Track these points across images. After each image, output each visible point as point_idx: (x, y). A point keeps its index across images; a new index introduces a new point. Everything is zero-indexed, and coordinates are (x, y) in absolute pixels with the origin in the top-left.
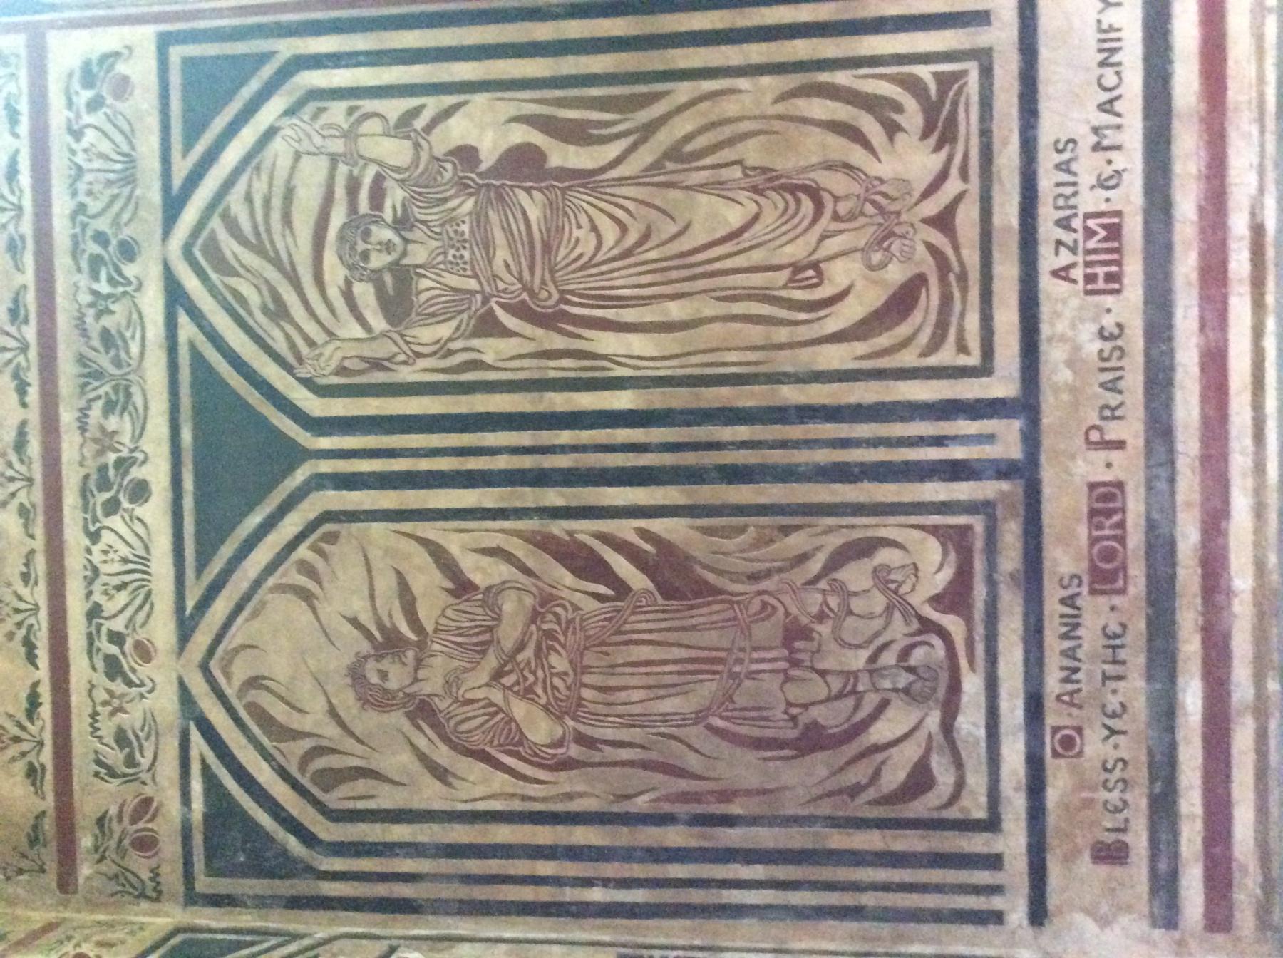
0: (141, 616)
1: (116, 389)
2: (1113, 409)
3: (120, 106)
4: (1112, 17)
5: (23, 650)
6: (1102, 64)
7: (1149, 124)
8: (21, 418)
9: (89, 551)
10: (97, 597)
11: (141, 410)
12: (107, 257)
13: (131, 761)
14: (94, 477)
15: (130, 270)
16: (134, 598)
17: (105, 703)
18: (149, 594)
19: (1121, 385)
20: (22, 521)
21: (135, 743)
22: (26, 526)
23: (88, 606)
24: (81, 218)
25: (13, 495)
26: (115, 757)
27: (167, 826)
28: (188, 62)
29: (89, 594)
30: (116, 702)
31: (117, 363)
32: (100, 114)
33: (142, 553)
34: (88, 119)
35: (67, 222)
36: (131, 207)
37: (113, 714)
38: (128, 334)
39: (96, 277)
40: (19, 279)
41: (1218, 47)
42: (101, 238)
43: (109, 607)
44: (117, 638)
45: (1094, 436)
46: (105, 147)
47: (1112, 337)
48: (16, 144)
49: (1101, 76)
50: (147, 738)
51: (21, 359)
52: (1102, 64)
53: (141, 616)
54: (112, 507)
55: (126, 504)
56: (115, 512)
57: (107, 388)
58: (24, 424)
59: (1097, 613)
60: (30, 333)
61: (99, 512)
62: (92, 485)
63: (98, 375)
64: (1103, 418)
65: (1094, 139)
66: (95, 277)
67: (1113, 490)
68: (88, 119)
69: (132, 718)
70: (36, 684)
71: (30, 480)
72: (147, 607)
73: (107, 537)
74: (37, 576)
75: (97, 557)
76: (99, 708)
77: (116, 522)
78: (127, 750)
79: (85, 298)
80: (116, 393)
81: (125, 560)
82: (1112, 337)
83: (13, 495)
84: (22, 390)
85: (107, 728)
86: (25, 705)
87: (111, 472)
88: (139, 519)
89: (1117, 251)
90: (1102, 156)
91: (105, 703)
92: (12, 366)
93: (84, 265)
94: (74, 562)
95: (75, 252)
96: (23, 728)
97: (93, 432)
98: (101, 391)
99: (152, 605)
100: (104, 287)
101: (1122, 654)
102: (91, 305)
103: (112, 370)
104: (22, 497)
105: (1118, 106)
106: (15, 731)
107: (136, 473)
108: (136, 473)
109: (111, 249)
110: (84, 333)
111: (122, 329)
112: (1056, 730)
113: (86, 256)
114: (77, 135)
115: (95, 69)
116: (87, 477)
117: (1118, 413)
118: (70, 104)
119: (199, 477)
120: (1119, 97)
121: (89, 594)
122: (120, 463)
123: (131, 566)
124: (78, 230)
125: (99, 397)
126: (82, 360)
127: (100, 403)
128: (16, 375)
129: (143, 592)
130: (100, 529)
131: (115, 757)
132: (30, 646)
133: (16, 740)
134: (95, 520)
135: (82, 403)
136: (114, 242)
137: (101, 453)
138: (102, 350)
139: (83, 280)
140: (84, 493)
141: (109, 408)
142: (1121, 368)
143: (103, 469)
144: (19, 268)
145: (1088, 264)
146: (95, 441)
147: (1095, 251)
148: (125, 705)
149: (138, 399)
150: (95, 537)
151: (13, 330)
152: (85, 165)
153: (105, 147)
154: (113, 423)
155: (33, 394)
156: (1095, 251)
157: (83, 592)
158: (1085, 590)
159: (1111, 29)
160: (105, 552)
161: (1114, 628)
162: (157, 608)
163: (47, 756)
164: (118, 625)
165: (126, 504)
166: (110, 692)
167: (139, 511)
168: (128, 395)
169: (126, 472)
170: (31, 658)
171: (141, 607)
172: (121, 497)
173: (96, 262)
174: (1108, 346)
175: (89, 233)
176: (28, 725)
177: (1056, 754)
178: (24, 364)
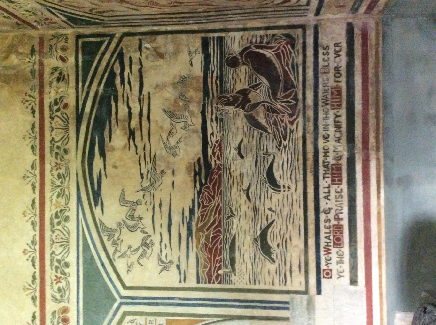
0: (66, 255)
1: (61, 190)
3: (65, 111)
5: (31, 263)
7: (353, 177)
8: (33, 198)
9: (51, 236)
10: (53, 136)
11: (68, 196)
12: (59, 153)
13: (62, 296)
15: (66, 157)
16: (65, 249)
18: (69, 248)
20: (32, 319)
21: (63, 291)
22: (33, 227)
23: (51, 252)
24: (53, 255)
26: (58, 296)
28: (83, 43)
29: (51, 135)
30: (58, 280)
34: (56, 227)
35: (49, 144)
38: (66, 175)
40: (35, 196)
41: (389, 314)
43: (56, 140)
44: (58, 147)
48: (35, 158)
50: (67, 290)
53: (66, 255)
54: (59, 223)
55: (62, 109)
56: (59, 112)
58: (35, 273)
60: (37, 247)
61: (54, 112)
62: (53, 216)
66: (56, 158)
71: (36, 215)
72: (68, 253)
74: (36, 242)
75: (54, 237)
76: (53, 281)
77: (60, 227)
78: (61, 294)
79: (54, 164)
81: (62, 239)
82: (326, 61)
84: (34, 188)
85: (56, 287)
87: (59, 214)
92: (32, 182)
93: (54, 270)
95: (51, 265)
97: (54, 202)
99: (69, 252)
100: (59, 275)
102: (55, 280)
105: (329, 198)
107: (66, 214)
108: (66, 214)
109: (61, 264)
110: (52, 175)
111: (64, 287)
112: (324, 270)
113: (54, 266)
114: (52, 119)
115: (58, 101)
116: (52, 215)
118: (51, 110)
119: (85, 303)
121: (51, 135)
122: (61, 211)
123: (63, 240)
124: (52, 145)
127: (57, 194)
128: (33, 185)
130: (55, 230)
131: (58, 296)
132: (33, 261)
134: (53, 113)
138: (57, 178)
139: (54, 159)
141: (58, 80)
142: (342, 201)
143: (57, 213)
144: (34, 193)
145: (332, 177)
146: (55, 205)
147: (335, 174)
148: (61, 167)
149: (67, 192)
150: (52, 119)
151: (32, 172)
152: (54, 127)
155: (37, 228)
156: (335, 174)
157: (50, 248)
158: (332, 244)
159: (338, 122)
160: (56, 236)
163: (38, 294)
164: (59, 257)
165: (62, 109)
166: (56, 276)
167: (67, 224)
168: (64, 192)
170: (34, 266)
171: (66, 253)
172: (61, 107)
173: (57, 268)
174: (338, 195)
175: (55, 146)
177: (324, 277)
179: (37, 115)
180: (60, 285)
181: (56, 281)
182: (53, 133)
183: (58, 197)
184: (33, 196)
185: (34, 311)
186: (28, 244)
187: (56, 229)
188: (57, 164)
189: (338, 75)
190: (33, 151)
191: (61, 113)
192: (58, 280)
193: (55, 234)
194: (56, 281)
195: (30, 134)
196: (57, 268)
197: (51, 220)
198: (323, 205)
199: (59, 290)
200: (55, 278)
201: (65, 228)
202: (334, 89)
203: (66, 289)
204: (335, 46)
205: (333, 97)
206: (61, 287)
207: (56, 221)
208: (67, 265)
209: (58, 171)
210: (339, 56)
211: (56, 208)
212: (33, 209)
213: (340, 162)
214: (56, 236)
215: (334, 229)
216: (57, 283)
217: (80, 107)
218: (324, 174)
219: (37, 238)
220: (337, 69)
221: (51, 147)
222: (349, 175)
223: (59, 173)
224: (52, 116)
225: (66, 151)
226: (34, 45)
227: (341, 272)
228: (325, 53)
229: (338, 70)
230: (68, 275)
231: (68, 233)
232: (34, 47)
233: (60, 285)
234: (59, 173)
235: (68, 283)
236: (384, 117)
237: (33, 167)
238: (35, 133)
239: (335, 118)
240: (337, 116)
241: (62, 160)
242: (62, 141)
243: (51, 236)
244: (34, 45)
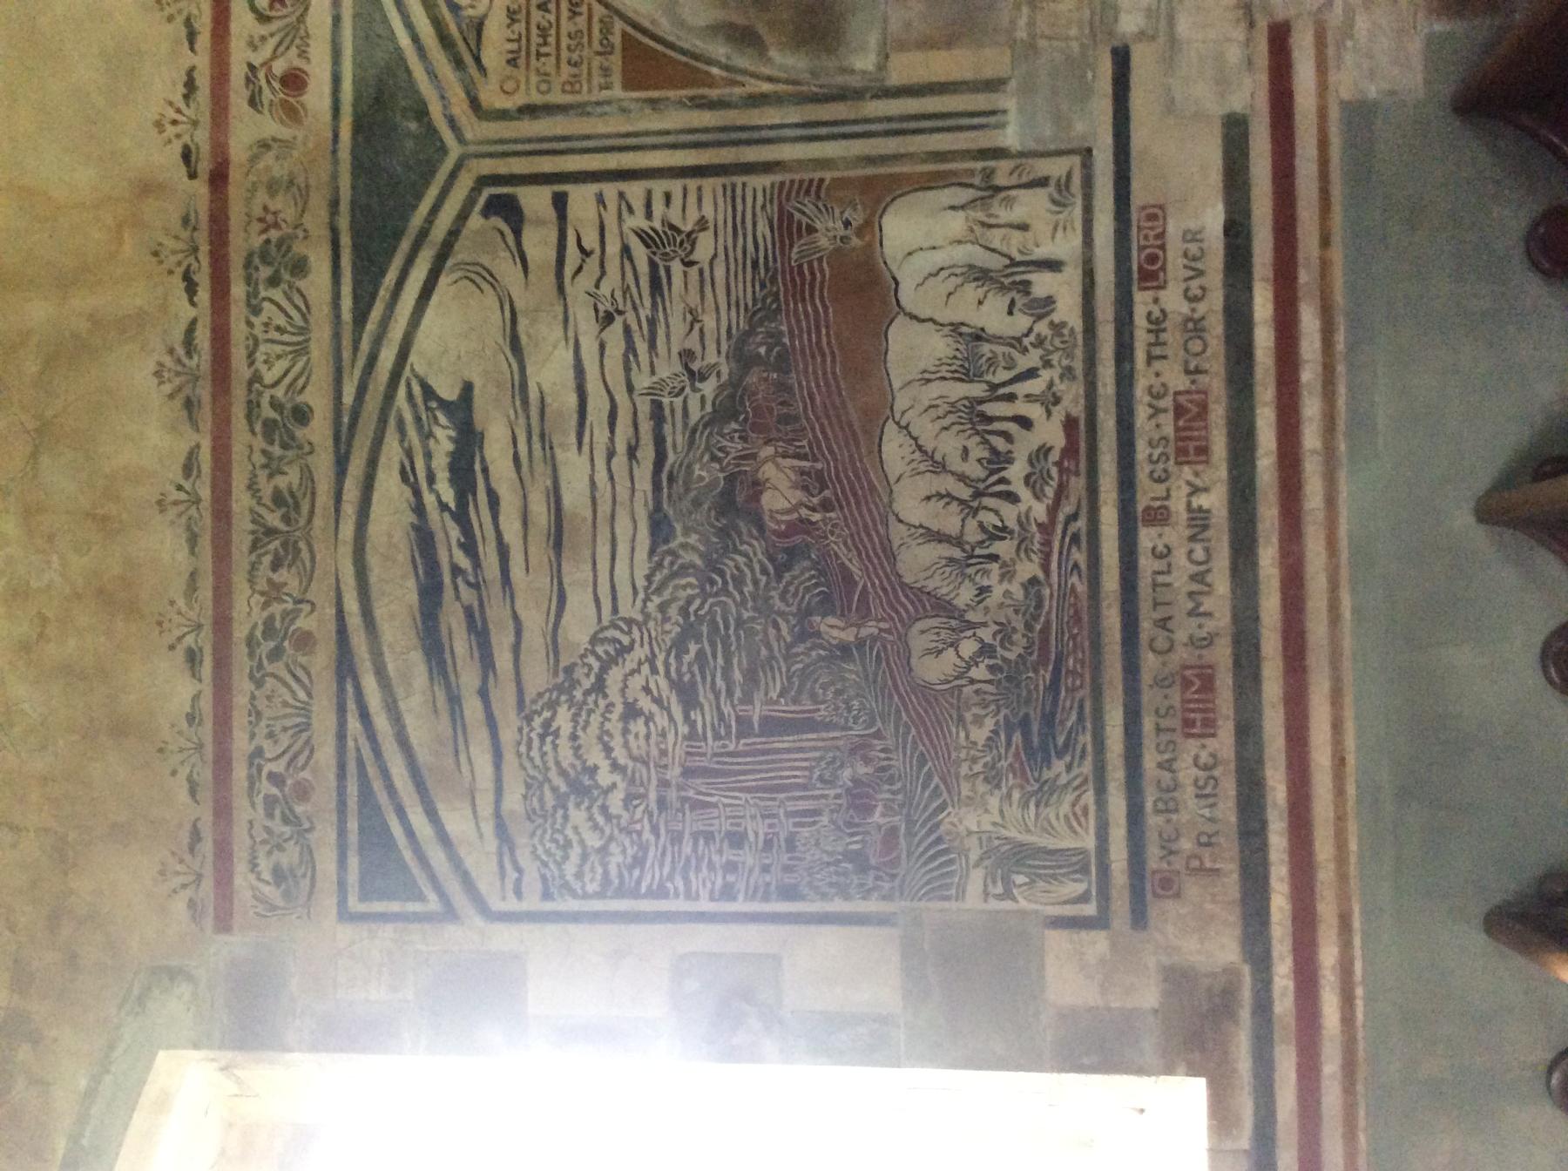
1: (285, 545)
2: (1210, 836)
4: (1203, 501)
5: (182, 285)
6: (1192, 538)
14: (260, 628)
15: (300, 433)
17: (264, 842)
19: (1209, 579)
25: (180, 639)
27: (317, 97)
31: (286, 519)
32: (281, 664)
33: (301, 324)
36: (306, 753)
37: (271, 476)
38: (299, 873)
39: (270, 815)
42: (275, 779)
43: (269, 378)
44: (275, 779)
45: (1195, 863)
46: (281, 321)
47: (1206, 768)
49: (1191, 552)
51: (193, 511)
52: (1192, 538)
54: (276, 654)
55: (286, 276)
57: (277, 543)
58: (194, 322)
59: (1146, 304)
62: (258, 633)
63: (271, 532)
64: (1200, 844)
65: (1190, 605)
66: (270, 815)
67: (1156, 210)
68: (269, 667)
69: (290, 478)
70: (192, 70)
73: (270, 683)
75: (258, 331)
77: (276, 294)
80: (286, 550)
81: (285, 704)
83: (180, 639)
86: (181, 90)
88: (304, 668)
89: (1206, 428)
90: (1194, 621)
91: (264, 842)
93: (258, 428)
94: (238, 331)
96: (179, 111)
98: (271, 547)
101: (1163, 336)
102: (265, 466)
103: (282, 527)
104: (189, 640)
106: (172, 114)
111: (295, 487)
112: (1154, 872)
114: (259, 684)
115: (278, 624)
116: (255, 626)
117: (1213, 840)
120: (1208, 571)
121: (251, 364)
124: (254, 770)
125: (266, 553)
126: (256, 519)
129: (304, 735)
133: (174, 122)
134: (260, 666)
135: (253, 557)
136: (289, 782)
137: (266, 605)
139: (259, 442)
140: (248, 264)
142: (1215, 795)
143: (270, 621)
146: (262, 594)
147: (1190, 701)
153: (281, 321)
154: (282, 575)
156: (1190, 701)
159: (1200, 509)
161: (1157, 313)
162: (314, 378)
164: (278, 767)
165: (286, 276)
166: (268, 830)
168: (298, 551)
169: (293, 621)
170: (192, 36)
173: (270, 427)
176: (185, 360)
178: (195, 12)
179: (204, 295)
180: (281, 482)
181: (268, 847)
182: (262, 730)
183: (275, 566)
184: (188, 59)
185: (187, 66)
186: (171, 104)
187: (264, 299)
188: (268, 830)
189: (1196, 346)
190: (192, 668)
191: (287, 666)
192: (273, 468)
193: (263, 317)
194: (268, 847)
195: (179, 361)
196: (270, 802)
197: (250, 641)
198: (1147, 493)
199: (278, 499)
200: (263, 460)
201: (300, 673)
202: (1196, 671)
203: (299, 495)
204: (1184, 240)
205: (1189, 695)
206: (285, 866)
207: (265, 272)
208: (302, 415)
209: (273, 482)
210: (1200, 273)
211: (265, 231)
212: (189, 354)
213: (1208, 656)
214: (266, 362)
215: (1143, 243)
216: (271, 476)
217: (344, 429)
218: (1150, 345)
219: (206, 705)
220: (1194, 327)
221: (251, 778)
222: (1240, 706)
223: (276, 487)
224: (254, 302)
225: (303, 792)
226: (198, 819)
227: (1194, 259)
228: (1155, 458)
229: (1195, 330)
230: (307, 448)
231: (303, 315)
232: (196, 74)
233: (281, 482)
234: (276, 487)
235: (308, 475)
236: (1352, 347)
237: (191, 718)
238: (196, 358)
239: (1191, 494)
240: (1195, 490)
241: (285, 446)
242: (287, 757)
243: (253, 697)
244: (198, 819)
